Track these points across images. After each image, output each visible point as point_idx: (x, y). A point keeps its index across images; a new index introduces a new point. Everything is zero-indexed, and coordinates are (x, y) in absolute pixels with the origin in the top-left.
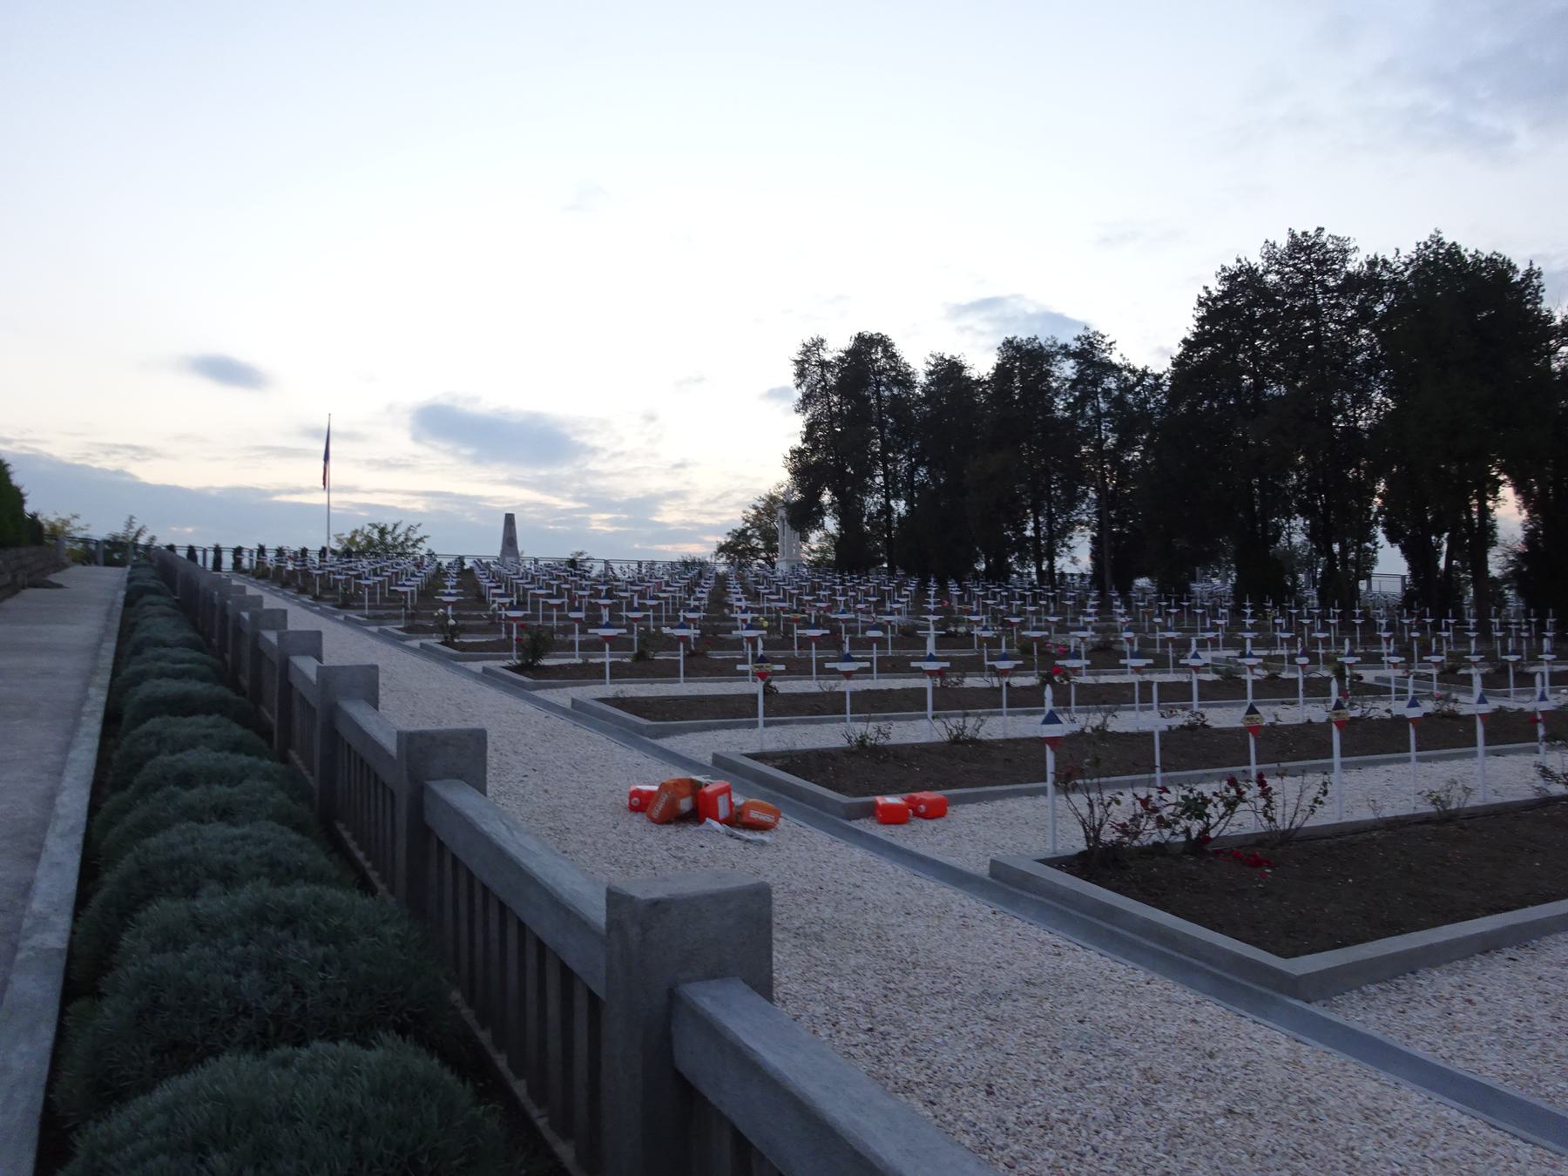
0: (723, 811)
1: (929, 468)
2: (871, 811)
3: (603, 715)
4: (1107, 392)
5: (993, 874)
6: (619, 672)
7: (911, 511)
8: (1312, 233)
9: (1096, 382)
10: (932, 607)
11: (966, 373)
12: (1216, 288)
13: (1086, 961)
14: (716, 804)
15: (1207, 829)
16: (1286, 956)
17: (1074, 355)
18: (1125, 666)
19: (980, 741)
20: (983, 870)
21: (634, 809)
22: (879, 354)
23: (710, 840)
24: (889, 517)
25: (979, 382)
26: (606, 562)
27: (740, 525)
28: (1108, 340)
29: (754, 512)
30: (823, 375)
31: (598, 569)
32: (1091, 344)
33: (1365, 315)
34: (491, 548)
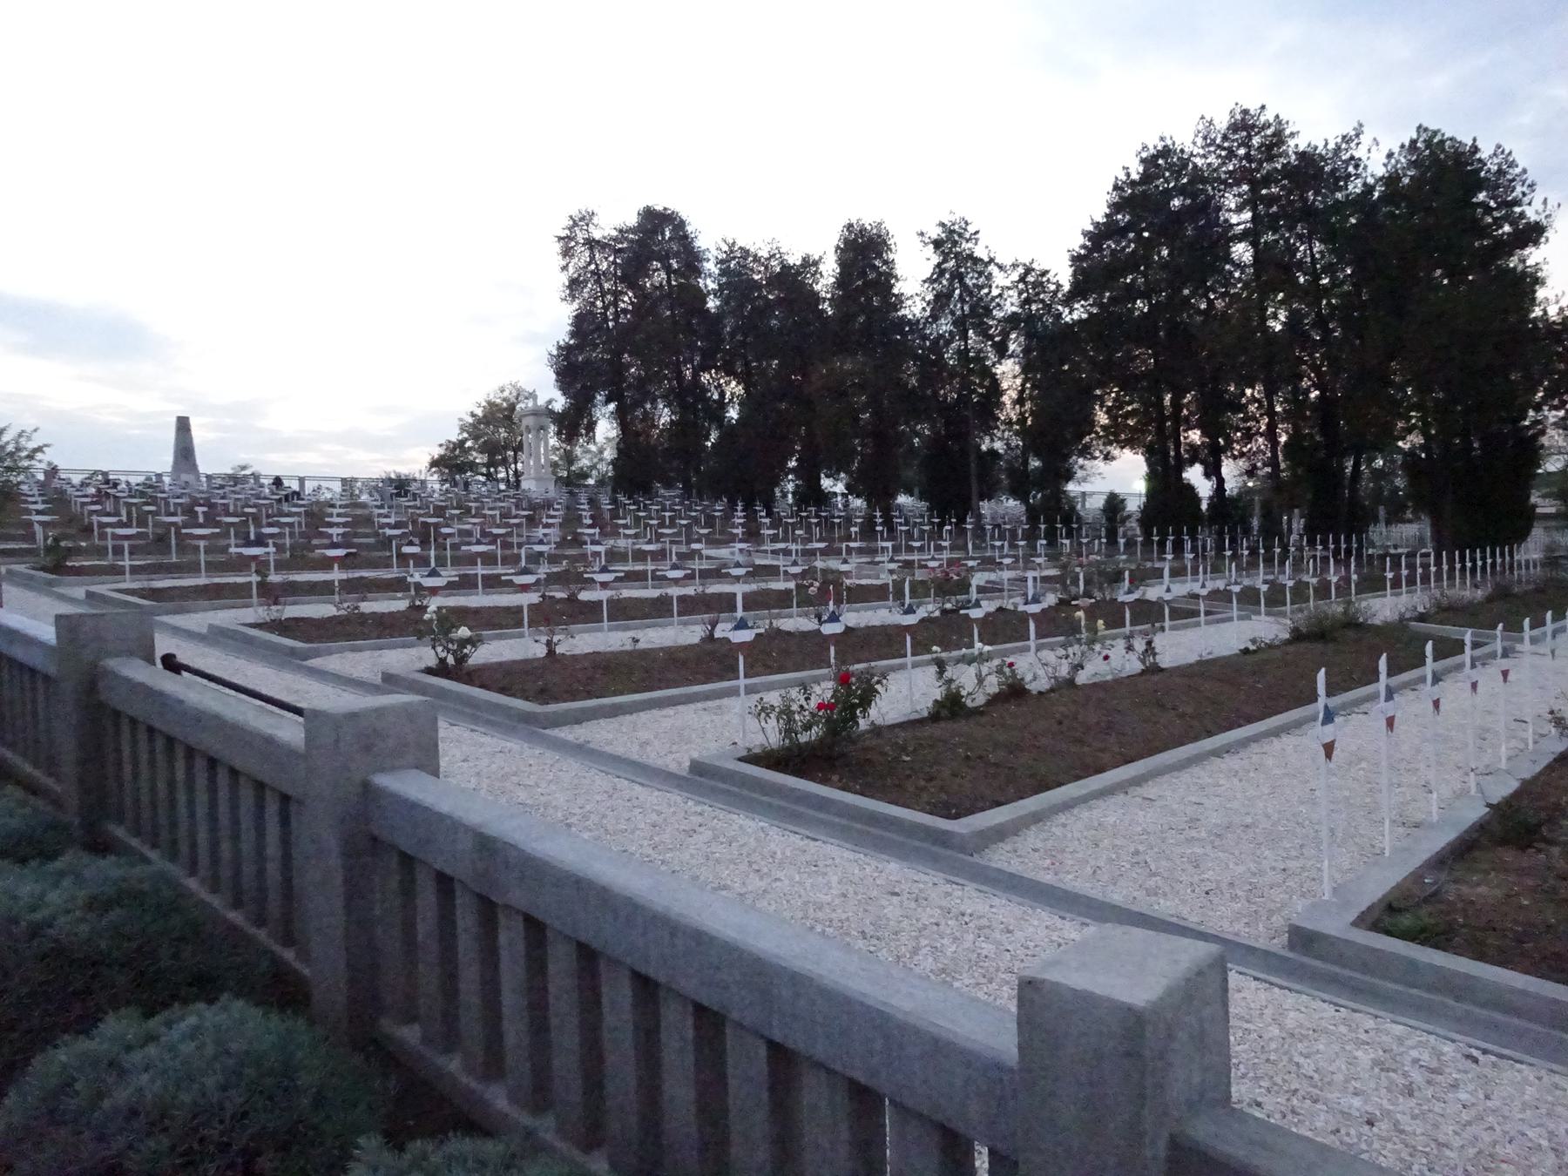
3: (249, 641)
5: (1292, 946)
10: (739, 531)
12: (689, 229)
13: (781, 841)
16: (957, 817)
26: (344, 481)
27: (455, 436)
28: (971, 229)
30: (592, 258)
34: (162, 461)
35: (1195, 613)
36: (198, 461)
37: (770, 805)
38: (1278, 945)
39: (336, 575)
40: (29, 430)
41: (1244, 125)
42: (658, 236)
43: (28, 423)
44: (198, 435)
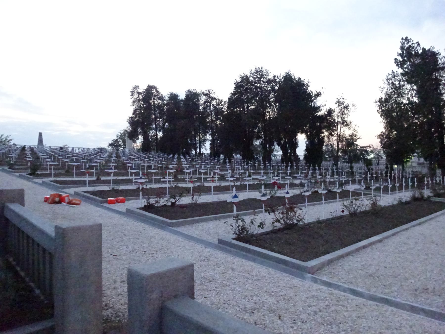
0: (67, 200)
1: (168, 124)
2: (107, 202)
3: (50, 184)
4: (213, 105)
5: (75, 194)
6: (56, 175)
7: (164, 135)
8: (260, 68)
9: (210, 103)
11: (179, 98)
12: (239, 80)
14: (65, 200)
15: (176, 201)
17: (205, 95)
18: (228, 180)
21: (45, 201)
22: (154, 91)
23: (63, 208)
24: (157, 137)
25: (182, 100)
27: (115, 138)
28: (213, 91)
29: (120, 134)
30: (138, 96)
31: (70, 149)
32: (209, 92)
33: (273, 89)
39: (111, 178)
41: (257, 71)
42: (149, 93)
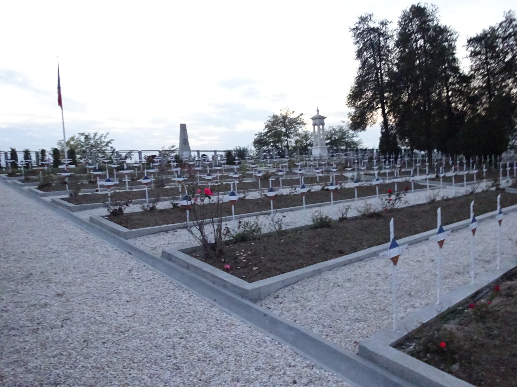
5: (162, 256)
19: (285, 232)
20: (350, 350)
34: (175, 142)
35: (425, 187)
36: (190, 146)
37: (100, 230)
38: (350, 350)
40: (105, 134)
43: (104, 132)
44: (189, 131)
